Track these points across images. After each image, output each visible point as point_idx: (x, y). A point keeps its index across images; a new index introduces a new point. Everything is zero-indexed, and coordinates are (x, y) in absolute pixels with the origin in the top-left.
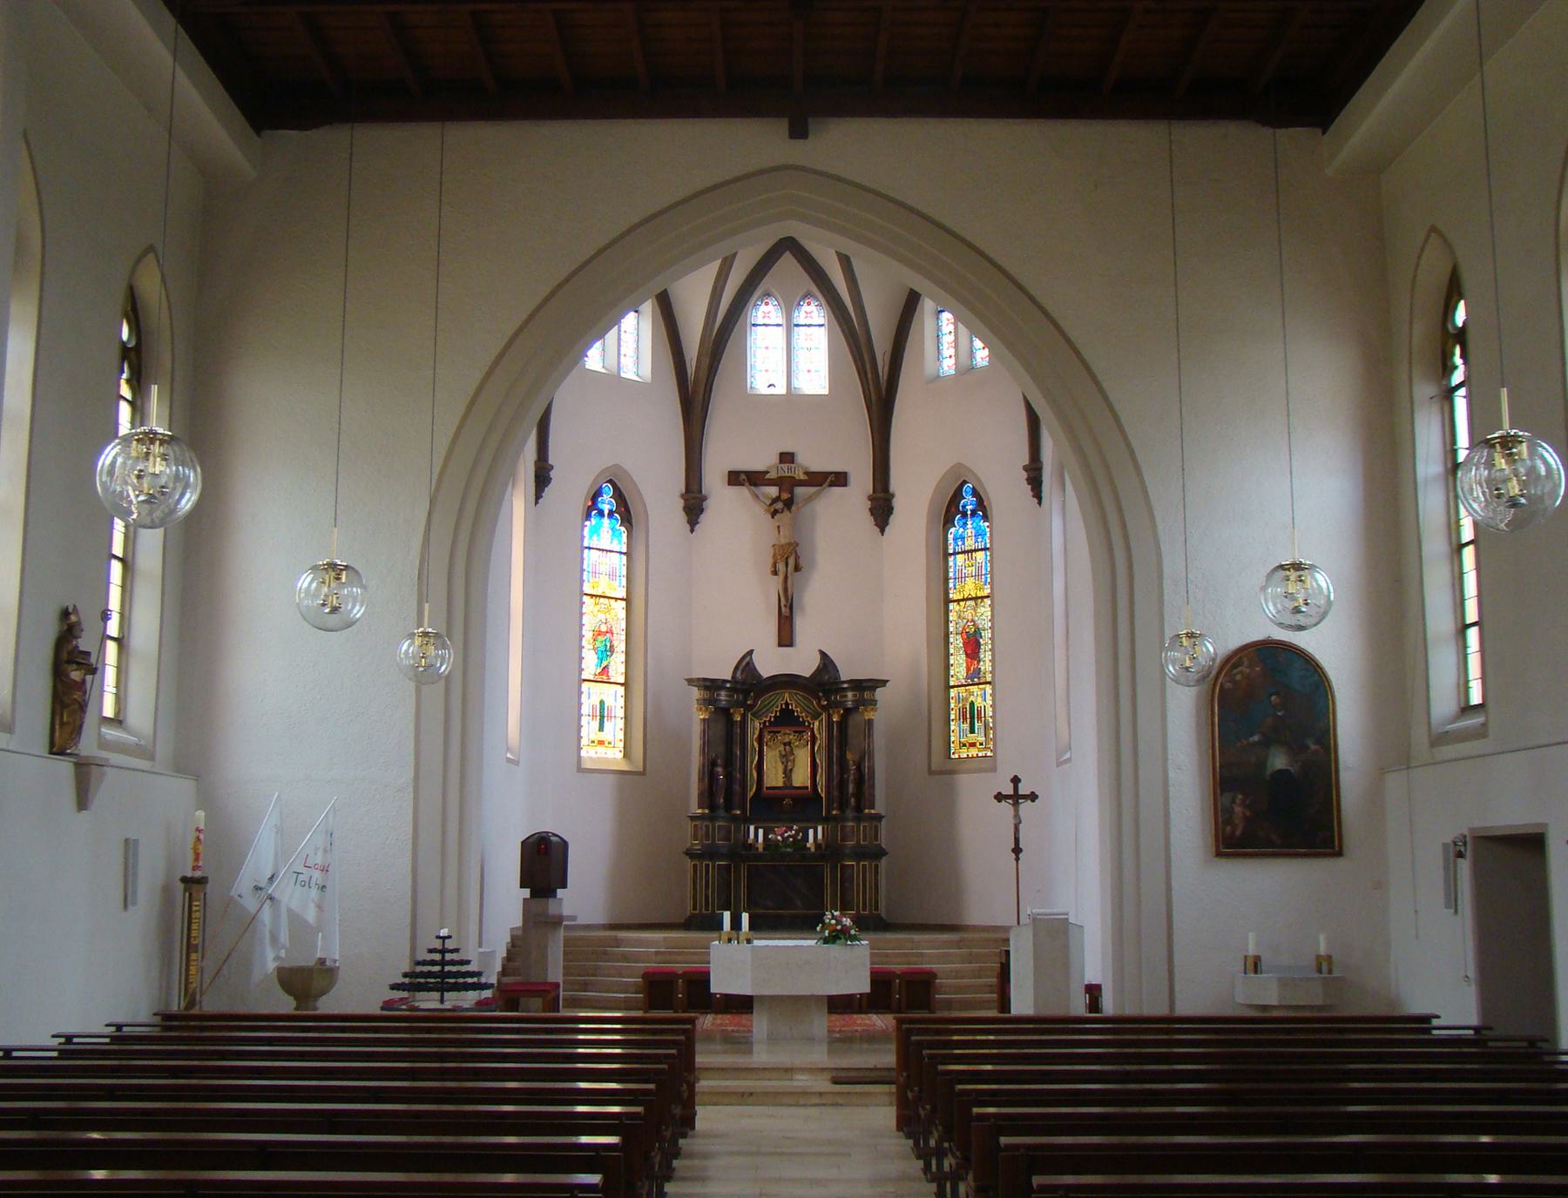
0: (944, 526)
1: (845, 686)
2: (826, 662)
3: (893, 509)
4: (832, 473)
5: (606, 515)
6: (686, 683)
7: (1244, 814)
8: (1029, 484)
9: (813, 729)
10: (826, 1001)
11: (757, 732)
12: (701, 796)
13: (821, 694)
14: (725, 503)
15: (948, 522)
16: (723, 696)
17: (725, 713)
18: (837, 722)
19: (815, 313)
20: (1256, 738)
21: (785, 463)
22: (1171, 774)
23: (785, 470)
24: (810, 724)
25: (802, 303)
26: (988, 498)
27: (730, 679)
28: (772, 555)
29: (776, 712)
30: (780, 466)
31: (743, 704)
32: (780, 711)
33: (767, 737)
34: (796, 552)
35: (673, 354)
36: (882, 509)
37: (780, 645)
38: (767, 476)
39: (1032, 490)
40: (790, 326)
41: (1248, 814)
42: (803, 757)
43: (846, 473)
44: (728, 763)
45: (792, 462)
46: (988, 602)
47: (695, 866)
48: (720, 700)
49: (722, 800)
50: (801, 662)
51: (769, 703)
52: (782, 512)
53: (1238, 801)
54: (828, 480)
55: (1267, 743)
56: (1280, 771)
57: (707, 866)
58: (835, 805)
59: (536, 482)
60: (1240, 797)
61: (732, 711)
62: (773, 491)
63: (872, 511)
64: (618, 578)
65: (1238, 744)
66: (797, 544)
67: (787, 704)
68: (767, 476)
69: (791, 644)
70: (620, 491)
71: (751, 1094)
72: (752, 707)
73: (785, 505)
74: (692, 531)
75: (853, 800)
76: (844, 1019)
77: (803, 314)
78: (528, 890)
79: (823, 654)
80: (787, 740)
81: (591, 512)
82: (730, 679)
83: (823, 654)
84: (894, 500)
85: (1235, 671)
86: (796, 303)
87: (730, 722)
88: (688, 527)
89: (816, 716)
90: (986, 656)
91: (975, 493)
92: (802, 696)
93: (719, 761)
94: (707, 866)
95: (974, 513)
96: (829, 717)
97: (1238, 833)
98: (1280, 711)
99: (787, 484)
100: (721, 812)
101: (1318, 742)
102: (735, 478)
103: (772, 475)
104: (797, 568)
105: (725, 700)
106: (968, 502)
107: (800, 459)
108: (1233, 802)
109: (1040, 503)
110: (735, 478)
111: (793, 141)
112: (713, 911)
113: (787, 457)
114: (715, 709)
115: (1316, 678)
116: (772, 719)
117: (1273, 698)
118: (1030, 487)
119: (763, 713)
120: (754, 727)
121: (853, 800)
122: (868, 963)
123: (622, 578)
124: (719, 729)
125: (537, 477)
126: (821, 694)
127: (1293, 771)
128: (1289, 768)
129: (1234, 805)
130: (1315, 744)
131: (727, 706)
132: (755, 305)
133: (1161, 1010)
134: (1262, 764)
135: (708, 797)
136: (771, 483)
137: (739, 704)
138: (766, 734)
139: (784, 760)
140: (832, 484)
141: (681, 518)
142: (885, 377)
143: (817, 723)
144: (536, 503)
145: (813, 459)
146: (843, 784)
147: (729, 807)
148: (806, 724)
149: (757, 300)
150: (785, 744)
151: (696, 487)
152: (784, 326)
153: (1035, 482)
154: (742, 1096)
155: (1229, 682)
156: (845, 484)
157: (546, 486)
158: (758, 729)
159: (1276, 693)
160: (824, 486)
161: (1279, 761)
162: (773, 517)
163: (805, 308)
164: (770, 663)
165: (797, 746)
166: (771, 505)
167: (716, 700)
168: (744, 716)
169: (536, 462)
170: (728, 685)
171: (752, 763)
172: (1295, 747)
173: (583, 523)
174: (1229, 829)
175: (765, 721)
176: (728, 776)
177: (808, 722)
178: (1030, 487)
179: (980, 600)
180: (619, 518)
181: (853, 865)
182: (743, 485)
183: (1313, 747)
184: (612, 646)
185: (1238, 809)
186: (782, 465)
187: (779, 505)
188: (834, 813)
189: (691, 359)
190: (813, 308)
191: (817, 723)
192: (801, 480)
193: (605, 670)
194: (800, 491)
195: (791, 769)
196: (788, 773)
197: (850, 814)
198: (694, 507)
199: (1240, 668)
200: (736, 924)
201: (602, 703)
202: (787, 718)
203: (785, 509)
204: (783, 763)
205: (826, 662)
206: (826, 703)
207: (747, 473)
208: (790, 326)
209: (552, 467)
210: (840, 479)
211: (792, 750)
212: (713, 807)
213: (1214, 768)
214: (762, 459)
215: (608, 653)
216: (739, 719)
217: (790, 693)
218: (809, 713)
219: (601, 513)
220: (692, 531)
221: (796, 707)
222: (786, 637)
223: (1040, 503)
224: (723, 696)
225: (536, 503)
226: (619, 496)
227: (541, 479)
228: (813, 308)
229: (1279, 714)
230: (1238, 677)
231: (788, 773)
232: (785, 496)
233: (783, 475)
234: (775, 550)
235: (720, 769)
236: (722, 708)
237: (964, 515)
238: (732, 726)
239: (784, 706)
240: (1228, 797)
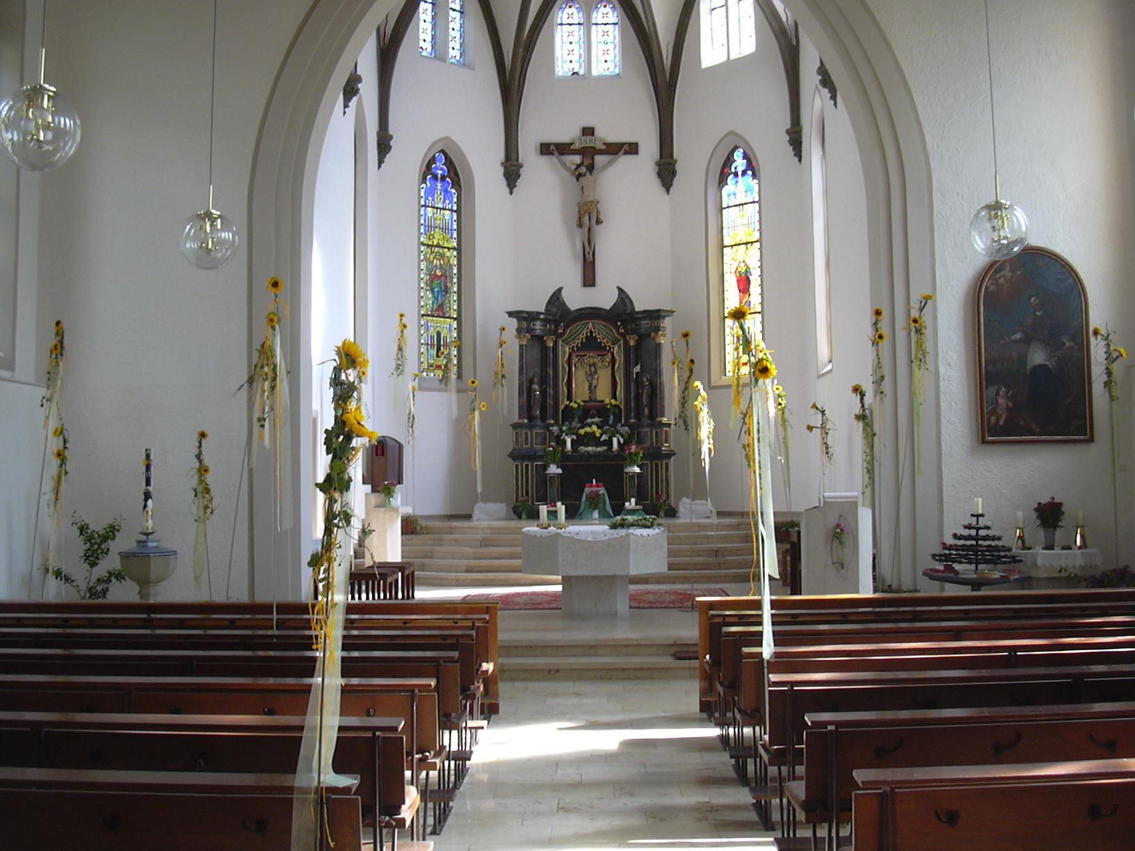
0: (719, 185)
1: (640, 315)
2: (623, 296)
3: (676, 172)
4: (626, 143)
5: (439, 179)
6: (507, 315)
7: (1007, 405)
8: (791, 145)
9: (613, 352)
10: (302, 724)
11: (567, 356)
12: (520, 408)
13: (619, 323)
14: (538, 171)
15: (722, 181)
16: (538, 325)
17: (540, 339)
18: (633, 346)
19: (611, 14)
20: (1017, 336)
21: (588, 135)
22: (942, 370)
23: (588, 142)
24: (610, 348)
25: (599, 6)
26: (756, 158)
27: (543, 311)
28: (577, 211)
29: (582, 339)
30: (583, 138)
31: (555, 333)
32: (586, 337)
33: (575, 360)
34: (597, 209)
35: (493, 47)
36: (666, 172)
37: (585, 285)
38: (572, 147)
39: (794, 150)
40: (587, 24)
41: (1010, 404)
42: (604, 376)
43: (637, 144)
44: (543, 381)
45: (593, 134)
46: (757, 245)
47: (517, 466)
48: (536, 329)
49: (538, 412)
50: (604, 297)
51: (576, 332)
52: (585, 176)
53: (1001, 393)
54: (623, 150)
55: (1027, 340)
56: (1040, 366)
57: (527, 466)
58: (632, 415)
59: (378, 149)
60: (1003, 389)
61: (545, 338)
62: (577, 159)
63: (659, 174)
64: (450, 232)
65: (1002, 342)
66: (598, 202)
67: (591, 332)
68: (572, 147)
69: (593, 285)
70: (451, 159)
71: (558, 671)
72: (562, 335)
73: (588, 169)
74: (511, 193)
75: (646, 410)
76: (1090, 669)
77: (600, 14)
78: (370, 486)
79: (620, 290)
80: (592, 362)
81: (427, 176)
82: (543, 311)
83: (620, 290)
84: (677, 164)
85: (998, 275)
86: (594, 6)
87: (544, 348)
88: (508, 190)
89: (616, 342)
90: (755, 288)
91: (745, 156)
92: (603, 325)
93: (536, 380)
94: (527, 466)
95: (744, 173)
96: (626, 343)
97: (1001, 423)
98: (1039, 311)
99: (589, 154)
100: (539, 423)
101: (1073, 339)
102: (546, 149)
103: (577, 146)
104: (599, 222)
105: (540, 330)
106: (739, 163)
107: (599, 133)
108: (997, 394)
109: (800, 160)
110: (546, 149)
111: (593, 126)
112: (533, 502)
113: (588, 131)
114: (532, 337)
115: (1071, 280)
116: (580, 345)
117: (1033, 299)
118: (820, 78)
119: (572, 340)
120: (564, 350)
121: (646, 410)
122: (665, 544)
123: (454, 232)
124: (535, 354)
125: (379, 145)
126: (619, 323)
127: (1050, 366)
128: (1047, 363)
129: (998, 397)
130: (1069, 341)
131: (542, 334)
132: (561, 8)
133: (240, 595)
134: (1023, 360)
135: (526, 408)
136: (575, 152)
137: (550, 333)
138: (574, 357)
139: (590, 379)
140: (626, 153)
141: (502, 182)
142: (669, 64)
143: (616, 348)
144: (379, 166)
145: (608, 133)
146: (638, 397)
147: (543, 418)
148: (608, 348)
149: (562, 4)
150: (590, 366)
151: (514, 157)
152: (585, 24)
153: (796, 141)
154: (549, 673)
155: (993, 284)
156: (636, 153)
157: (387, 153)
158: (568, 353)
159: (1037, 295)
160: (620, 153)
161: (1038, 357)
162: (578, 180)
163: (602, 10)
164: (576, 299)
165: (600, 367)
166: (576, 169)
167: (533, 329)
168: (556, 343)
169: (378, 133)
170: (542, 317)
171: (563, 379)
172: (1052, 343)
173: (419, 186)
174: (993, 419)
175: (573, 347)
176: (543, 392)
177: (609, 346)
178: (791, 147)
179: (750, 244)
180: (450, 182)
181: (648, 464)
182: (552, 154)
183: (1068, 344)
184: (446, 287)
185: (1001, 401)
186: (585, 137)
187: (583, 170)
188: (632, 421)
189: (508, 52)
190: (608, 9)
191: (616, 348)
192: (600, 150)
193: (441, 307)
194: (599, 159)
195: (595, 387)
196: (592, 389)
197: (646, 421)
198: (512, 172)
199: (1003, 272)
200: (553, 514)
201: (439, 334)
202: (591, 344)
203: (588, 173)
204: (588, 381)
205: (623, 296)
206: (623, 331)
207: (557, 145)
208: (587, 24)
209: (391, 137)
210: (633, 149)
211: (596, 370)
212: (531, 418)
213: (980, 365)
214: (567, 133)
215: (444, 293)
216: (551, 345)
217: (593, 324)
218: (610, 339)
219: (435, 177)
220: (511, 193)
221: (599, 334)
222: (589, 279)
223: (800, 160)
224: (538, 325)
225: (379, 166)
226: (449, 163)
227: (383, 146)
228: (608, 9)
229: (1038, 314)
230: (1001, 281)
231: (592, 389)
232: (587, 162)
233: (586, 145)
234: (580, 206)
235: (536, 387)
236: (537, 336)
237: (736, 175)
238: (546, 351)
239: (589, 334)
240: (992, 390)
